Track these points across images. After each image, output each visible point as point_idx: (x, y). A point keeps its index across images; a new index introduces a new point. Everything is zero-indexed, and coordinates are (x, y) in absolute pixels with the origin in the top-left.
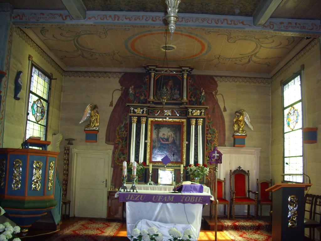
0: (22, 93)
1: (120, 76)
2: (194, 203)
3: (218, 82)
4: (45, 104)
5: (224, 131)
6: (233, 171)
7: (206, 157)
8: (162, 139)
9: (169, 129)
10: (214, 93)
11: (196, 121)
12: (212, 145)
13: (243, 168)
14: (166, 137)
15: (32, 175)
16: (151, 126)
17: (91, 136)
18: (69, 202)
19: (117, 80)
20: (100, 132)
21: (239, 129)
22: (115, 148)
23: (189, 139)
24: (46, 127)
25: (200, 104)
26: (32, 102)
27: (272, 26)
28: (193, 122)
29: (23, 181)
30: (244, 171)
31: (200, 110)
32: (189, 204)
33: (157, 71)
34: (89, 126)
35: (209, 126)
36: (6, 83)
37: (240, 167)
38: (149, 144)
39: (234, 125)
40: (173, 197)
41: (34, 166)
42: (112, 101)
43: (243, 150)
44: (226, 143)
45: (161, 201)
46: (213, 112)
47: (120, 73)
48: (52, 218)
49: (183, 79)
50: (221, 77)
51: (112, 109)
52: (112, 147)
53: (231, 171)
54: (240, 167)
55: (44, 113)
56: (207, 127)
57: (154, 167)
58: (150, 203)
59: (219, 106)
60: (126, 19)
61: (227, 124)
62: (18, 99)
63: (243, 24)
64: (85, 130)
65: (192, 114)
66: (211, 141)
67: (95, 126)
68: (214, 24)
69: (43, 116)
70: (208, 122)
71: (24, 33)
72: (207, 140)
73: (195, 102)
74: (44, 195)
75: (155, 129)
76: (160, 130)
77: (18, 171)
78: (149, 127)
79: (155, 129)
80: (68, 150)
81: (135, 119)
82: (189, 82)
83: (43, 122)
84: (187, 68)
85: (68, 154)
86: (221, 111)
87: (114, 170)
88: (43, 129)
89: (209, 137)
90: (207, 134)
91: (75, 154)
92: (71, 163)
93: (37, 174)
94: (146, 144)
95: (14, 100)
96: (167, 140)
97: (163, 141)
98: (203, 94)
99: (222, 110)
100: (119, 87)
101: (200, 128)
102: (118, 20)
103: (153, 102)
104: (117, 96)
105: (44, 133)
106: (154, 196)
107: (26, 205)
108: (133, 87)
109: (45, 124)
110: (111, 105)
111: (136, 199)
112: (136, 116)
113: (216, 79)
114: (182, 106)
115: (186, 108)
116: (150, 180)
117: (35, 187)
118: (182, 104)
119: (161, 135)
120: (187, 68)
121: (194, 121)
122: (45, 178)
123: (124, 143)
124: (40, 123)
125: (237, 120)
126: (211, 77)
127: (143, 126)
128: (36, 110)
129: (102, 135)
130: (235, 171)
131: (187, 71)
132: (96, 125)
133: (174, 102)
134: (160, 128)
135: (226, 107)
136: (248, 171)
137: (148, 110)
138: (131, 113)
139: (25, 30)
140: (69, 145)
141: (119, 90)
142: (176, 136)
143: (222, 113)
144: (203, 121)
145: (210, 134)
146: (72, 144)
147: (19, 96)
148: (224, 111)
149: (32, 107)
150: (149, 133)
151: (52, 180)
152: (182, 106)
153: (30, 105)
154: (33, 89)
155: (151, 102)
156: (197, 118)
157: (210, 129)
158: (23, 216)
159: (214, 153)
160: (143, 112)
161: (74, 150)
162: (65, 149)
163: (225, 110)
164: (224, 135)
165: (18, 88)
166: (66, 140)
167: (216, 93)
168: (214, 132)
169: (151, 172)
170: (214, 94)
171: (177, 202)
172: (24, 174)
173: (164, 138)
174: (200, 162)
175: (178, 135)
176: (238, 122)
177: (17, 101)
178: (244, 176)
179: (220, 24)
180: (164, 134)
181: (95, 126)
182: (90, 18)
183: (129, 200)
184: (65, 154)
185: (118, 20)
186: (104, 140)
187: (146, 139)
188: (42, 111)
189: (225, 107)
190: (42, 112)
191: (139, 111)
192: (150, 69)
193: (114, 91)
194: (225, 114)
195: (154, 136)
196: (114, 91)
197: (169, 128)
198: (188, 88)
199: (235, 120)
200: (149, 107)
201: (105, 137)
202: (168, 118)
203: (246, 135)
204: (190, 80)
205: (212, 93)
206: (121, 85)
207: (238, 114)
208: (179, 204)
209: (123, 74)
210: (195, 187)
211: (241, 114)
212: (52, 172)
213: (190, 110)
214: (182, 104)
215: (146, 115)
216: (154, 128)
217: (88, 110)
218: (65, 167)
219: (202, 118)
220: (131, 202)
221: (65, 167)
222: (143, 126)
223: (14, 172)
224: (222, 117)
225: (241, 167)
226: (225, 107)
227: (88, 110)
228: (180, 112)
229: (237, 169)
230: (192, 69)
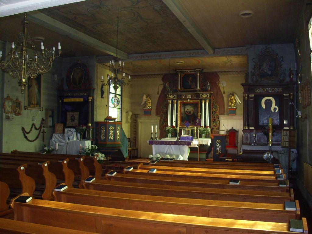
0: (105, 94)
1: (162, 76)
2: (184, 145)
3: (220, 76)
4: (119, 97)
5: (224, 105)
6: (228, 130)
7: (211, 122)
8: (187, 112)
9: (191, 106)
10: (217, 83)
11: (205, 101)
12: (216, 114)
13: (235, 128)
14: (189, 111)
15: (109, 133)
16: (180, 105)
17: (147, 113)
18: (137, 149)
19: (161, 78)
20: (152, 110)
21: (231, 105)
22: (161, 118)
23: (201, 112)
24: (121, 109)
25: (207, 91)
26: (111, 98)
27: (218, 53)
28: (203, 101)
29: (106, 136)
30: (235, 130)
31: (207, 94)
32: (182, 146)
33: (182, 72)
34: (146, 106)
35: (214, 103)
36: (97, 92)
37: (233, 128)
38: (179, 115)
39: (229, 103)
40: (174, 142)
41: (110, 129)
42: (158, 91)
43: (235, 117)
44: (225, 113)
45: (168, 144)
46: (217, 94)
47: (162, 74)
48: (122, 154)
49: (197, 76)
50: (222, 72)
51: (158, 96)
52: (159, 118)
53: (227, 130)
54: (233, 128)
55: (119, 102)
56: (212, 104)
57: (180, 129)
58: (163, 145)
59: (220, 91)
60: (147, 57)
61: (225, 101)
62: (103, 98)
63: (203, 54)
64: (144, 109)
65: (202, 97)
66: (215, 112)
67: (149, 107)
68: (188, 55)
69: (118, 104)
70: (213, 101)
71: (105, 65)
72: (212, 112)
73: (204, 90)
74: (115, 141)
75: (183, 106)
76: (186, 107)
77: (103, 131)
78: (179, 106)
79: (183, 106)
80: (136, 120)
81: (170, 102)
82: (201, 77)
83: (119, 106)
84: (199, 69)
85: (136, 123)
86: (222, 93)
87: (161, 131)
88: (119, 110)
89: (214, 110)
90: (212, 108)
91: (140, 123)
92: (138, 127)
93: (111, 132)
94: (177, 116)
95: (101, 98)
96: (190, 112)
97: (188, 113)
98: (208, 85)
99: (223, 93)
100: (162, 83)
101: (207, 104)
102: (143, 58)
103: (180, 91)
104: (161, 88)
105: (120, 112)
106: (165, 142)
107: (107, 146)
108: (168, 83)
109: (120, 108)
110: (158, 93)
111: (157, 143)
112: (170, 100)
113: (219, 74)
114: (197, 93)
115: (199, 93)
116: (178, 136)
117: (111, 138)
118: (196, 91)
119: (186, 110)
120: (199, 69)
121: (204, 101)
122: (115, 134)
123: (165, 115)
124: (117, 107)
125: (231, 99)
126: (216, 73)
127: (175, 105)
128: (114, 101)
129: (154, 111)
130: (230, 130)
131: (199, 71)
132: (149, 106)
133: (192, 90)
134: (185, 106)
135: (225, 91)
136: (238, 130)
137: (178, 96)
138: (167, 98)
139: (105, 64)
140: (136, 118)
141: (162, 84)
142: (195, 110)
143: (222, 95)
144: (209, 101)
145: (214, 108)
146: (137, 117)
147: (103, 96)
148: (224, 94)
149: (112, 100)
150: (179, 109)
151: (119, 135)
152: (197, 93)
153: (110, 99)
154: (111, 91)
155: (179, 91)
156: (205, 99)
157: (214, 105)
158: (107, 151)
159: (197, 120)
160: (174, 97)
161: (139, 121)
162: (134, 120)
163: (224, 93)
164: (224, 108)
165: (102, 93)
166: (134, 115)
167: (219, 83)
168: (216, 107)
169: (178, 131)
170: (217, 83)
171: (176, 145)
172: (106, 132)
173: (188, 112)
174: (208, 125)
175: (196, 109)
176: (231, 100)
177: (103, 99)
178: (235, 133)
179: (191, 55)
180: (188, 109)
181: (149, 107)
182: (130, 58)
183: (154, 144)
184: (134, 123)
185: (143, 58)
186: (155, 114)
187: (177, 112)
188: (118, 101)
189: (224, 91)
190: (118, 102)
191: (172, 97)
192: (178, 72)
193: (160, 85)
194: (224, 95)
195: (182, 110)
196: (160, 85)
197: (190, 105)
198: (201, 81)
199: (229, 99)
200: (177, 94)
201: (155, 112)
202: (189, 100)
203: (236, 108)
204: (202, 76)
205: (216, 83)
206: (163, 82)
207: (231, 95)
208: (177, 145)
209: (164, 75)
210: (188, 137)
211: (233, 95)
212: (119, 131)
213: (201, 95)
214: (196, 91)
215: (177, 99)
216: (182, 106)
217: (145, 97)
218: (134, 130)
219: (208, 99)
220: (155, 145)
221: (134, 130)
222: (175, 105)
223: (101, 132)
224: (223, 97)
225: (227, 129)
226: (224, 91)
227: (145, 97)
228: (196, 96)
229: (231, 129)
230: (203, 69)
